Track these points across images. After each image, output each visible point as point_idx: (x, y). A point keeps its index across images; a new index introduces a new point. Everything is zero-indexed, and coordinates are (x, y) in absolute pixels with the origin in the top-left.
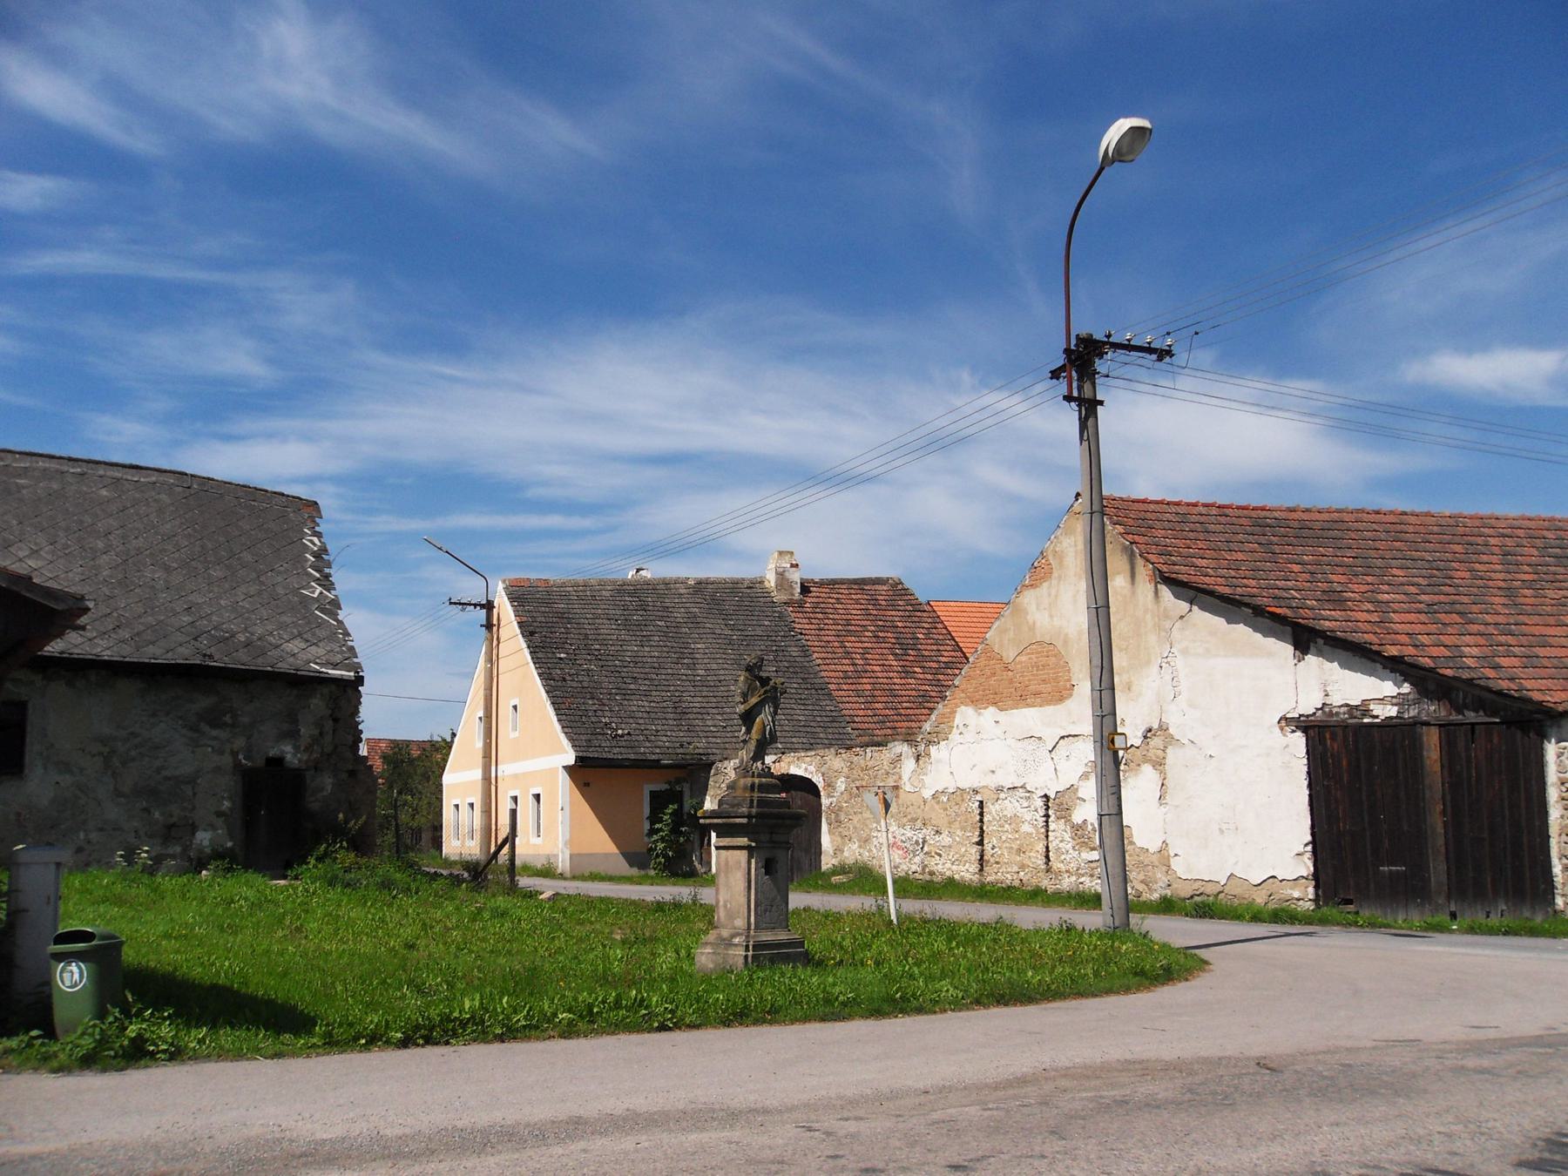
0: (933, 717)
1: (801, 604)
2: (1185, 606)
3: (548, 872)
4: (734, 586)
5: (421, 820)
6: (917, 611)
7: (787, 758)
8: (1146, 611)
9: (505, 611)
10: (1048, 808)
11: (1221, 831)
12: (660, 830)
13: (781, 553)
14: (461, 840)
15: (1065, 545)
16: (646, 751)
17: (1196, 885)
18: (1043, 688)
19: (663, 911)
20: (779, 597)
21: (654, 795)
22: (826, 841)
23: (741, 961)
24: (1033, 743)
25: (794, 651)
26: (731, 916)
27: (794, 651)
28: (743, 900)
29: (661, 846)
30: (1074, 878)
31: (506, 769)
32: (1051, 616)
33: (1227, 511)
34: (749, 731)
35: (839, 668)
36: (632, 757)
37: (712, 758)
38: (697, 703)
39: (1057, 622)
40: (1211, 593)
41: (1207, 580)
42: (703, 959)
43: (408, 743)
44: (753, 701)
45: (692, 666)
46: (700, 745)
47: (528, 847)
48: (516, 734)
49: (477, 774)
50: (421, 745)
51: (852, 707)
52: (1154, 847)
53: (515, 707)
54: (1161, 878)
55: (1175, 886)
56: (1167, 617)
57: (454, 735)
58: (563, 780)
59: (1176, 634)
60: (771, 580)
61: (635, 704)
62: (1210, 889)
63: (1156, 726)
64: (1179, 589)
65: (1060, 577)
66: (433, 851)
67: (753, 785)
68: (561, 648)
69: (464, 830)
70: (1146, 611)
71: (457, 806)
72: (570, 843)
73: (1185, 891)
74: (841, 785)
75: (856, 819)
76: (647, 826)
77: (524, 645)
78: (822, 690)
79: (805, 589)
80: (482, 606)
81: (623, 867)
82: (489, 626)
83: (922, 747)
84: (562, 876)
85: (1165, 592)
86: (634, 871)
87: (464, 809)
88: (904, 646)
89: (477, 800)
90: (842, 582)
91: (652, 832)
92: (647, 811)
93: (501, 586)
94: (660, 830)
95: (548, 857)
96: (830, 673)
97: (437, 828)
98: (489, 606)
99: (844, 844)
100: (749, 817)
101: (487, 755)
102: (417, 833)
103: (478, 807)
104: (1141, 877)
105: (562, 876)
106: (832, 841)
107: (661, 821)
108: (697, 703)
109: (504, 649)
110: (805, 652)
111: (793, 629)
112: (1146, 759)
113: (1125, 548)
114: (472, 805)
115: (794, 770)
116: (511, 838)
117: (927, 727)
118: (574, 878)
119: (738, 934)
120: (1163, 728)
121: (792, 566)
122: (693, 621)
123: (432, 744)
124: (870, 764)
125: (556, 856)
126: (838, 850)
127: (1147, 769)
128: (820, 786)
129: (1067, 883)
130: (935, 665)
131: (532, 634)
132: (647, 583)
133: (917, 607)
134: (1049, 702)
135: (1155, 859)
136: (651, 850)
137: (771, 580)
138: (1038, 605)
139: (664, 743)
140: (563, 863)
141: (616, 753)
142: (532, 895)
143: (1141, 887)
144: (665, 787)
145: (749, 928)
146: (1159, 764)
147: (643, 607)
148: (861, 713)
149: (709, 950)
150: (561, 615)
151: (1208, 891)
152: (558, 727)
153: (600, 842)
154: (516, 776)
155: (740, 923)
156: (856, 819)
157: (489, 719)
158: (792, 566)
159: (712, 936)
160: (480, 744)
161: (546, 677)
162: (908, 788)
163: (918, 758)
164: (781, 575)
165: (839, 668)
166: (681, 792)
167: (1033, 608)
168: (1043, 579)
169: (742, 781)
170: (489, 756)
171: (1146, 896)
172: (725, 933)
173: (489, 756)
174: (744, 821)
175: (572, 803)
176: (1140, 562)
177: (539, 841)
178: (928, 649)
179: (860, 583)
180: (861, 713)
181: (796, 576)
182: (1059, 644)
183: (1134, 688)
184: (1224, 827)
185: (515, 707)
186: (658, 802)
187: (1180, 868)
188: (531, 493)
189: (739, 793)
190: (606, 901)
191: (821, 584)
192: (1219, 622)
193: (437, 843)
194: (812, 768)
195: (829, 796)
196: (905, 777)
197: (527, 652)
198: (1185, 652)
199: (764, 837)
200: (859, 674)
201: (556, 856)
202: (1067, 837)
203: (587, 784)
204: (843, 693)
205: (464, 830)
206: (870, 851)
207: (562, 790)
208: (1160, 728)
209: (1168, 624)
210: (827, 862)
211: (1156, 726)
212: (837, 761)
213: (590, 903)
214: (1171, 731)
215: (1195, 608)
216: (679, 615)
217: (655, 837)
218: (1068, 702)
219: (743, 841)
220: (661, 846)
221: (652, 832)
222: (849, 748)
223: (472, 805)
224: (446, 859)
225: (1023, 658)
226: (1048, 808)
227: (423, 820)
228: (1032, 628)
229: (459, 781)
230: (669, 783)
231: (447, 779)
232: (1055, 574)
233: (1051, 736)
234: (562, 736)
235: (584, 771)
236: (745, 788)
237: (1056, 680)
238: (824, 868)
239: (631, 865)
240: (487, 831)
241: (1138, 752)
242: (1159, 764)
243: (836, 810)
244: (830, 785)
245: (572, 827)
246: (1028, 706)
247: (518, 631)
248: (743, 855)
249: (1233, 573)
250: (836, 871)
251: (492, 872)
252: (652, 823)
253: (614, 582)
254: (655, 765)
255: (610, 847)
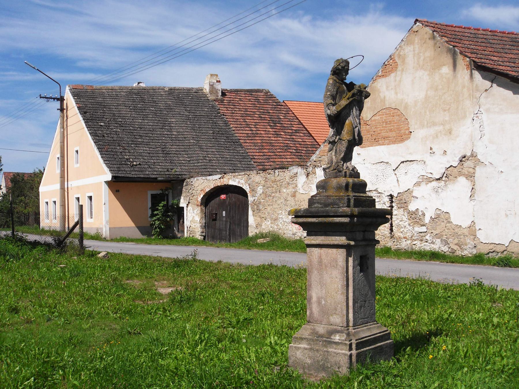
0: (317, 152)
1: (222, 101)
2: (488, 83)
3: (97, 237)
4: (188, 91)
5: (29, 210)
6: (278, 105)
7: (227, 177)
8: (464, 87)
9: (70, 101)
10: (392, 202)
11: (507, 215)
12: (157, 214)
13: (212, 75)
14: (49, 218)
15: (406, 51)
16: (149, 173)
17: (492, 246)
18: (390, 134)
19: (178, 266)
20: (211, 97)
21: (153, 196)
22: (252, 220)
23: (344, 361)
24: (383, 166)
25: (221, 123)
26: (325, 312)
27: (221, 123)
28: (341, 298)
29: (157, 223)
30: (409, 242)
31: (73, 184)
32: (396, 93)
33: (496, 34)
34: (338, 132)
35: (244, 132)
36: (142, 176)
37: (184, 177)
38: (174, 148)
39: (400, 96)
40: (506, 76)
41: (501, 67)
42: (299, 354)
43: (23, 174)
44: (344, 102)
45: (170, 130)
46: (177, 170)
47: (90, 224)
48: (78, 165)
49: (58, 186)
50: (30, 175)
51: (253, 151)
52: (465, 224)
53: (77, 152)
54: (470, 242)
55: (478, 247)
56: (477, 90)
57: (44, 169)
58: (105, 188)
59: (482, 100)
60: (207, 89)
61: (142, 149)
62: (499, 249)
63: (469, 154)
64: (486, 73)
65: (403, 70)
66: (35, 225)
67: (347, 185)
68: (102, 121)
69: (51, 216)
70: (464, 87)
71: (47, 203)
72: (109, 222)
73: (484, 250)
74: (260, 190)
75: (269, 208)
76: (150, 212)
77: (81, 119)
78: (237, 142)
79: (223, 94)
80: (58, 99)
81: (138, 235)
82: (62, 110)
83: (310, 169)
84: (105, 240)
85: (477, 74)
86: (145, 237)
87: (51, 204)
88: (274, 122)
89: (58, 200)
90: (241, 91)
91: (153, 215)
92: (150, 205)
93: (67, 88)
94: (157, 214)
95: (97, 229)
96: (240, 134)
97: (37, 214)
98: (61, 99)
99: (262, 222)
100: (352, 216)
101: (62, 176)
102: (27, 216)
103: (58, 204)
104: (456, 241)
105: (105, 240)
106: (255, 220)
107: (157, 210)
108: (174, 148)
109: (70, 113)
110: (226, 123)
111: (219, 113)
112: (460, 174)
113: (449, 50)
114: (55, 202)
115: (231, 183)
116: (80, 222)
117: (314, 157)
118: (112, 240)
119: (336, 332)
120: (473, 155)
121: (217, 82)
122: (169, 108)
123: (35, 174)
124: (278, 178)
125: (102, 229)
126: (258, 226)
127: (462, 180)
128: (248, 190)
129: (404, 245)
130: (290, 131)
131: (85, 113)
132: (144, 89)
133: (278, 103)
134: (394, 142)
135: (466, 232)
136: (152, 225)
137: (207, 89)
138: (387, 87)
139: (159, 169)
140: (105, 232)
141: (133, 174)
142: (93, 254)
143: (455, 247)
144: (159, 192)
145: (348, 326)
146: (470, 176)
147: (143, 100)
148: (257, 154)
149: (304, 345)
150: (100, 104)
151: (498, 250)
152: (101, 161)
153: (125, 222)
154: (78, 187)
155: (337, 320)
156: (269, 208)
157: (63, 158)
158: (217, 82)
159: (305, 331)
160: (58, 171)
161: (94, 135)
162: (301, 191)
163: (308, 175)
164: (212, 86)
165: (244, 132)
166: (167, 195)
167: (384, 88)
168: (391, 71)
169: (334, 182)
170: (63, 177)
171: (459, 253)
172: (321, 329)
173: (63, 177)
174: (346, 220)
175: (110, 201)
176: (460, 57)
177: (92, 220)
178: (286, 124)
179: (250, 91)
180: (257, 154)
181: (219, 87)
182: (402, 110)
183: (453, 132)
184: (508, 213)
185: (77, 152)
186: (156, 200)
187: (482, 236)
188: (80, 64)
189: (331, 192)
190: (139, 258)
191: (231, 91)
192: (508, 93)
193: (37, 221)
194: (242, 181)
195: (253, 196)
196: (300, 185)
197: (83, 122)
198: (488, 110)
199: (359, 236)
200: (255, 135)
201: (102, 229)
202: (405, 218)
203: (118, 191)
204: (247, 145)
205: (51, 216)
206: (278, 225)
207: (104, 196)
208: (472, 155)
209: (478, 95)
210: (252, 232)
211: (469, 154)
212: (257, 178)
213: (133, 260)
214: (479, 157)
215: (495, 85)
216: (162, 105)
217: (155, 218)
218: (407, 142)
219: (342, 240)
220: (157, 223)
221: (153, 215)
222: (264, 170)
223: (55, 202)
224: (43, 229)
225: (377, 118)
226: (392, 202)
227: (30, 210)
228: (383, 100)
229: (48, 190)
230: (162, 190)
231: (42, 189)
232: (400, 68)
233: (395, 161)
234: (104, 166)
235: (117, 184)
236: (339, 188)
237: (399, 129)
238: (250, 234)
239: (143, 234)
240: (64, 217)
241: (455, 170)
242: (470, 176)
243: (257, 204)
244: (253, 190)
245: (110, 214)
246: (380, 144)
247: (78, 111)
248: (342, 252)
249: (513, 65)
250: (256, 237)
251: (68, 241)
252: (153, 211)
253: (127, 88)
254: (155, 180)
255: (130, 223)
